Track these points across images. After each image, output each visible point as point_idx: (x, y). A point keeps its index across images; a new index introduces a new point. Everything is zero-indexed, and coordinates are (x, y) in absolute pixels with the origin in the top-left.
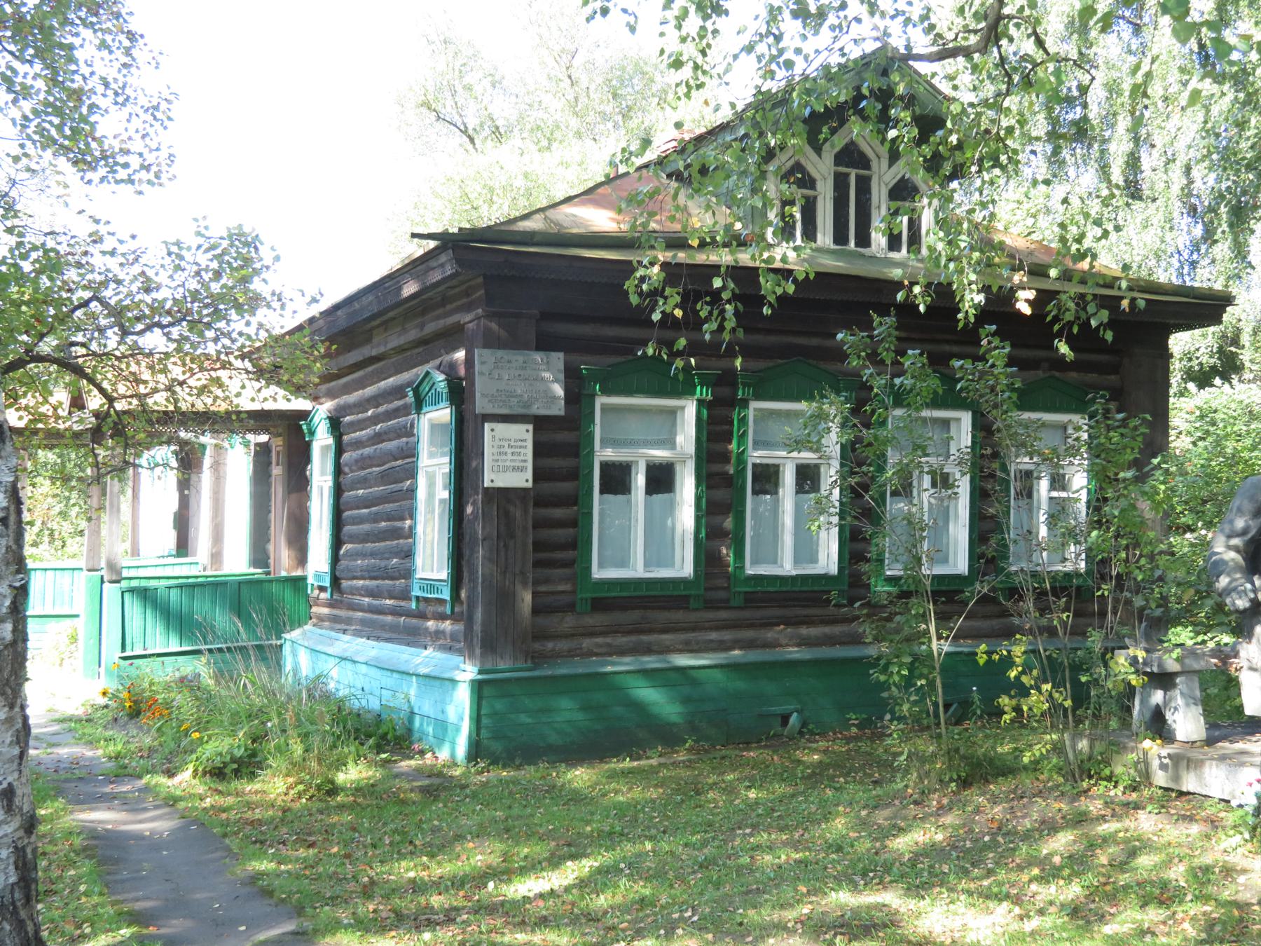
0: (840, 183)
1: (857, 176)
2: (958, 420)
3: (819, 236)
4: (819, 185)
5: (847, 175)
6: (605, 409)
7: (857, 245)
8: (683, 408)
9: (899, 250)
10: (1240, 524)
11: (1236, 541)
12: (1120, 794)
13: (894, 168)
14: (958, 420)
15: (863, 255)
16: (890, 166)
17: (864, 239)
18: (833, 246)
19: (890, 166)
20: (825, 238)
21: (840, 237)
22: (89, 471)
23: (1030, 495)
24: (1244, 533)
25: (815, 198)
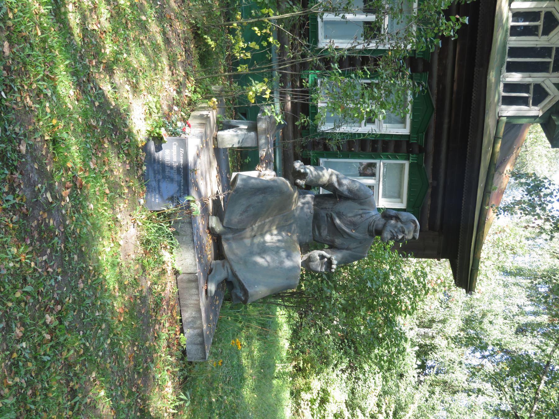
0: (545, 51)
1: (549, 63)
2: (405, 128)
3: (514, 38)
4: (545, 38)
5: (550, 57)
6: (403, 165)
7: (508, 63)
8: (402, 202)
9: (504, 91)
10: (345, 182)
11: (334, 179)
12: (186, 94)
13: (553, 87)
14: (405, 128)
15: (502, 66)
16: (554, 84)
17: (512, 68)
18: (508, 46)
19: (554, 84)
20: (515, 42)
21: (514, 52)
22: (368, 318)
23: (360, 176)
24: (340, 184)
25: (537, 35)
